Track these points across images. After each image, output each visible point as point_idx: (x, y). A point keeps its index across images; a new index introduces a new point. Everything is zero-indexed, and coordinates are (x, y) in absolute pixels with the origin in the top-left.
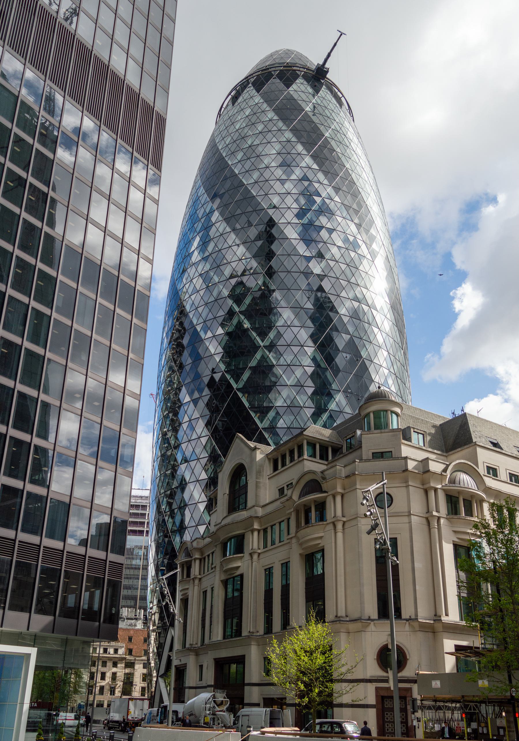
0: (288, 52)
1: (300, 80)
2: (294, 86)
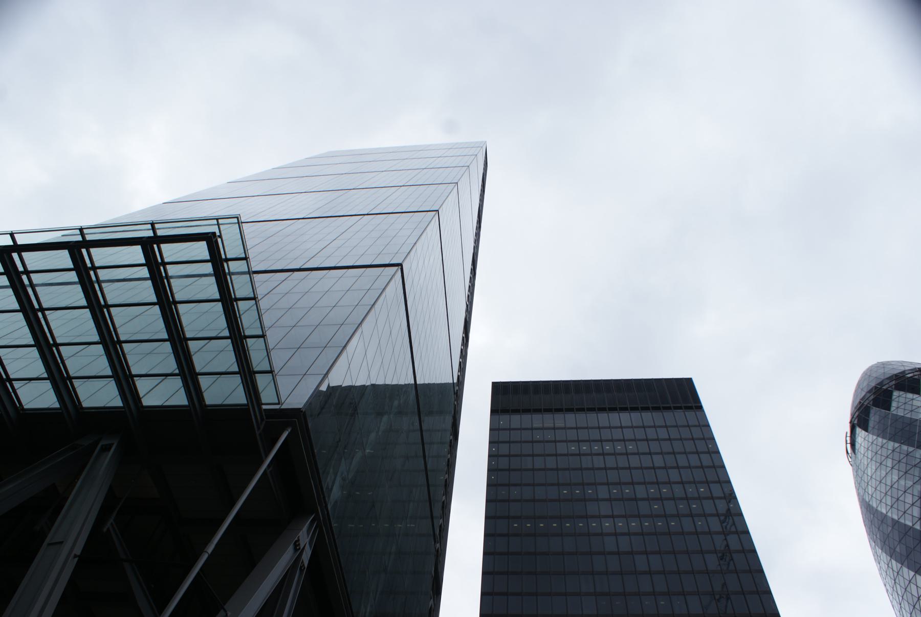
0: (867, 374)
1: (896, 394)
2: (894, 404)
